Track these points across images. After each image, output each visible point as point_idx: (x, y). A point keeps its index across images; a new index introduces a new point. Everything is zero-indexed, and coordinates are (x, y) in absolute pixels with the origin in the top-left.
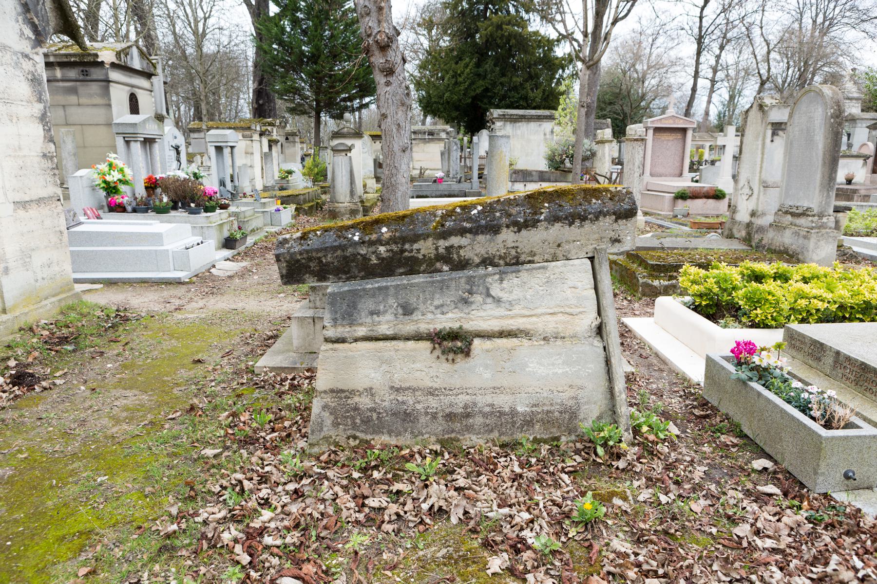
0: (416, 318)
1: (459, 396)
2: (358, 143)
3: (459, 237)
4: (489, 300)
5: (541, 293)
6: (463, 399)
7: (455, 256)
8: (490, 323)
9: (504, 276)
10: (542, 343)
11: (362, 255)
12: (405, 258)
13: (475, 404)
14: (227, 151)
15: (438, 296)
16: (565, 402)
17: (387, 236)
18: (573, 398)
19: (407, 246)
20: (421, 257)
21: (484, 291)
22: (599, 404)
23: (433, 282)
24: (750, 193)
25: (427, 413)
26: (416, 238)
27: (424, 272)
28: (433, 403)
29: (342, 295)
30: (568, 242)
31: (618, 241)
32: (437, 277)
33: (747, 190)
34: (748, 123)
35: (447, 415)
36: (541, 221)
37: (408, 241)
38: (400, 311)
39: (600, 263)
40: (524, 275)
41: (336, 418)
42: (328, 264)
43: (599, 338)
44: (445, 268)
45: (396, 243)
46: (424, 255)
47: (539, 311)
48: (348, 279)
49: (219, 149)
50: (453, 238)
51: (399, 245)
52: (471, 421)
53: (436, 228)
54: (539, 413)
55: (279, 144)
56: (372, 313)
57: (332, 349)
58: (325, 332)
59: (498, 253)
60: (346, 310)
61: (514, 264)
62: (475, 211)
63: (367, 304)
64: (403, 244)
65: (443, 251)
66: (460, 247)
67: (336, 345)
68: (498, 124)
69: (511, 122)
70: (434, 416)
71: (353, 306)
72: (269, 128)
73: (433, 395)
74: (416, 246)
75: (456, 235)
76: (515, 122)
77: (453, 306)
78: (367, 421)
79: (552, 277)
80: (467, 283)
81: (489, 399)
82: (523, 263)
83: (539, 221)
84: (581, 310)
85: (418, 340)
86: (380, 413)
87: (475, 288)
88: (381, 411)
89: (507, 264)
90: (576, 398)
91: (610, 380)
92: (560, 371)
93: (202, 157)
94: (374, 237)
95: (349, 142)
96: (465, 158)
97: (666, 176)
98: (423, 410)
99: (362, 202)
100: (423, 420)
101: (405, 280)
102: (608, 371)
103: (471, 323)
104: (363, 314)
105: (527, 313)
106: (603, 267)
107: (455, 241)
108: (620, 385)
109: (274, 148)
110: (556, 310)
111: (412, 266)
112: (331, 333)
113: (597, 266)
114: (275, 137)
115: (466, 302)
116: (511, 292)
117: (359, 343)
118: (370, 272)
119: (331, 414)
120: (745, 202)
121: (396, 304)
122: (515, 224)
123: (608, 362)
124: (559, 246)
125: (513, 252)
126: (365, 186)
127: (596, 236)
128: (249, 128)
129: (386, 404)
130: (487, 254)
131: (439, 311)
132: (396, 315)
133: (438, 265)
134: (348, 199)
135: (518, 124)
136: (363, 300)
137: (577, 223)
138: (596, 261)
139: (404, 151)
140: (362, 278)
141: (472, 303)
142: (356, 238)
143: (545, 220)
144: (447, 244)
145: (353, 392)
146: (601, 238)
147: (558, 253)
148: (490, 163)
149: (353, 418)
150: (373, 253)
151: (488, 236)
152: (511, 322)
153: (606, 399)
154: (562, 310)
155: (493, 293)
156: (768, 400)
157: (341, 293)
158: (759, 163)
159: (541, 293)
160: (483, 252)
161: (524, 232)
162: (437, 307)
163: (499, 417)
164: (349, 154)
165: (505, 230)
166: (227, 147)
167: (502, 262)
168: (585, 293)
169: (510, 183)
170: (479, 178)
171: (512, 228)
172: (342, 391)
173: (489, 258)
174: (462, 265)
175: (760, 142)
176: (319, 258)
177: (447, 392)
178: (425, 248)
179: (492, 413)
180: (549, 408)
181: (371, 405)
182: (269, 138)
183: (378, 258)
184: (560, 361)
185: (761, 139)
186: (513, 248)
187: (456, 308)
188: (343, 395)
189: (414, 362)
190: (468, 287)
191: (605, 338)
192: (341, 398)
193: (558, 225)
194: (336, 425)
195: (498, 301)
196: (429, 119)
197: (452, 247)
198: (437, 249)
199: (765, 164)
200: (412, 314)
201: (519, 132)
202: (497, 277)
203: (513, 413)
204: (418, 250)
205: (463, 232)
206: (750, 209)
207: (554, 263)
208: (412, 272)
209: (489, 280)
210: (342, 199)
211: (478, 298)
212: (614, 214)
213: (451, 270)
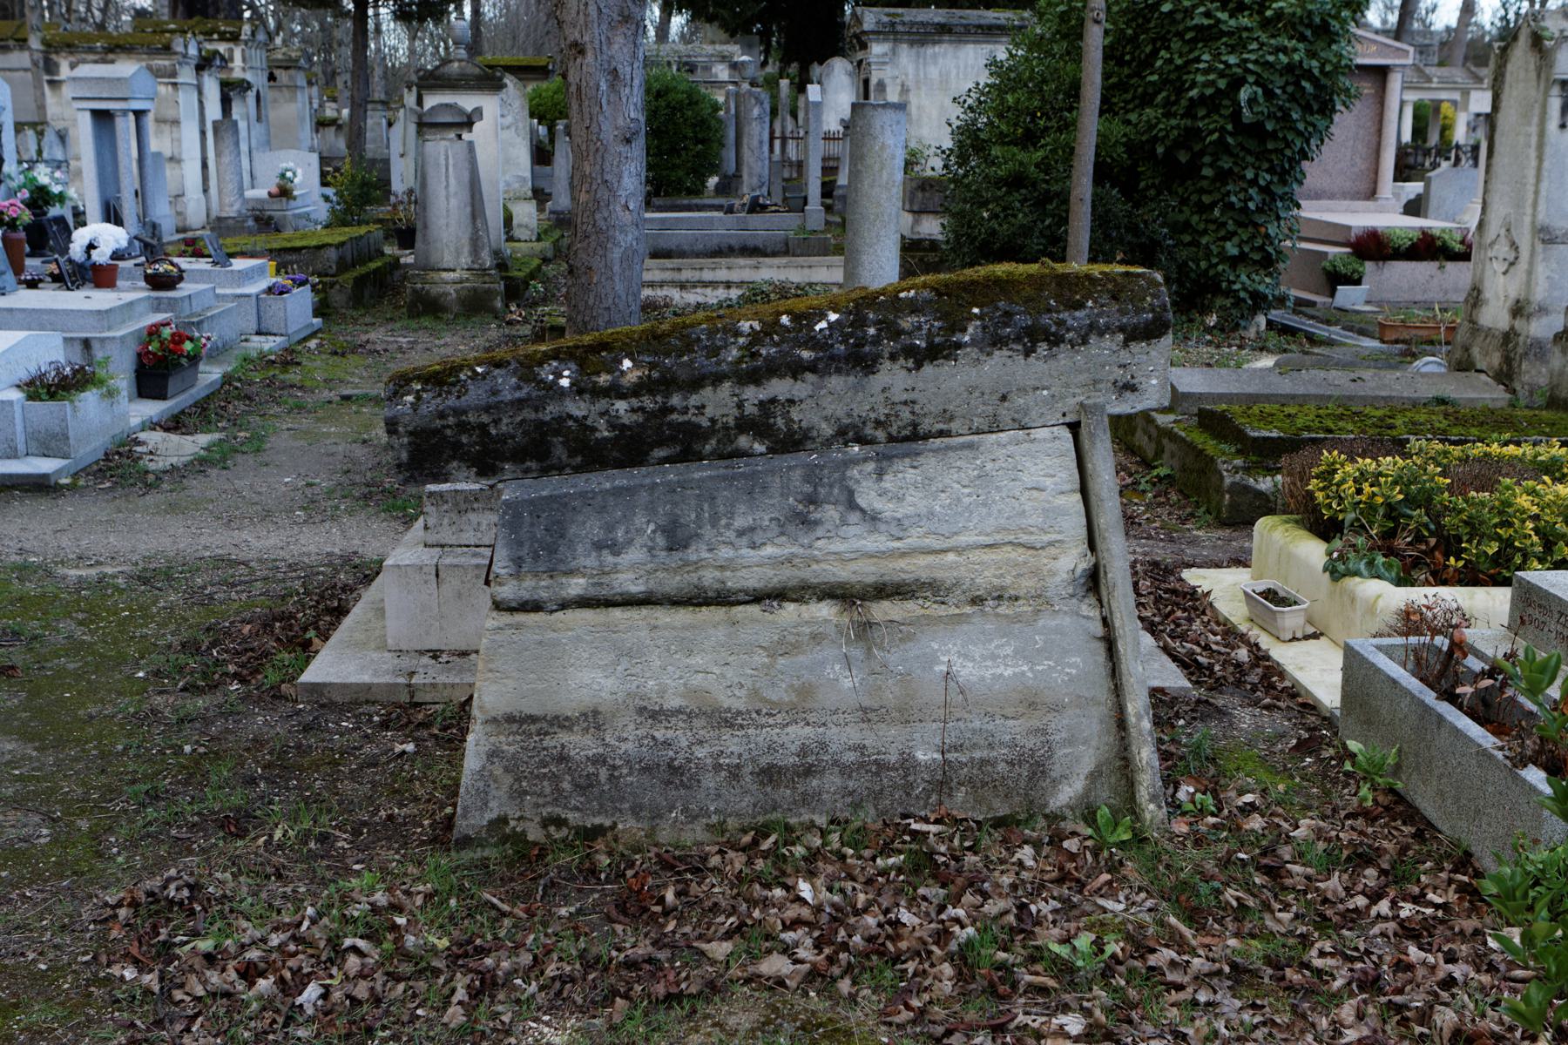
0: (694, 557)
1: (789, 729)
2: (488, 103)
3: (789, 381)
4: (854, 517)
5: (966, 500)
6: (798, 733)
7: (780, 422)
8: (854, 566)
9: (885, 464)
10: (968, 609)
11: (576, 420)
12: (671, 425)
13: (823, 746)
14: (125, 127)
15: (742, 508)
16: (1020, 740)
17: (633, 377)
18: (1037, 730)
19: (676, 400)
20: (705, 423)
21: (843, 498)
22: (1094, 743)
23: (733, 478)
24: (1511, 258)
25: (718, 767)
26: (696, 384)
27: (709, 457)
28: (733, 744)
29: (537, 507)
30: (1022, 390)
31: (1130, 387)
32: (742, 466)
33: (1503, 249)
34: (1508, 77)
35: (763, 771)
36: (966, 345)
37: (680, 388)
38: (661, 541)
39: (1092, 435)
40: (930, 463)
41: (518, 780)
42: (502, 439)
43: (1092, 600)
44: (759, 447)
45: (652, 392)
46: (713, 421)
47: (964, 539)
48: (545, 472)
49: (103, 118)
50: (775, 381)
51: (659, 399)
52: (815, 783)
53: (740, 360)
54: (962, 765)
55: (251, 95)
56: (599, 546)
57: (510, 626)
58: (495, 588)
59: (873, 415)
60: (539, 539)
61: (906, 439)
62: (823, 325)
63: (589, 527)
64: (667, 396)
65: (755, 410)
66: (791, 402)
67: (520, 617)
68: (877, 49)
69: (912, 43)
70: (734, 773)
71: (558, 531)
72: (222, 48)
73: (732, 726)
74: (694, 400)
75: (781, 377)
76: (923, 43)
77: (777, 530)
78: (586, 786)
79: (989, 466)
80: (807, 479)
81: (853, 734)
82: (926, 437)
83: (959, 345)
84: (1054, 537)
85: (700, 605)
86: (614, 767)
87: (822, 491)
88: (618, 762)
89: (891, 439)
90: (1044, 732)
91: (1118, 690)
92: (1008, 672)
93: (40, 134)
94: (604, 379)
95: (467, 101)
96: (784, 140)
97: (1332, 197)
98: (709, 761)
99: (502, 266)
100: (710, 781)
101: (672, 473)
102: (1114, 670)
103: (815, 567)
104: (580, 548)
105: (936, 543)
106: (1099, 445)
107: (779, 388)
108: (1137, 707)
109: (237, 111)
110: (998, 538)
111: (688, 444)
112: (507, 591)
113: (1086, 444)
114: (237, 74)
115: (806, 522)
116: (900, 499)
117: (569, 612)
118: (592, 454)
119: (506, 770)
120: (1502, 279)
121: (652, 527)
122: (909, 351)
123: (1110, 643)
124: (1004, 398)
125: (906, 414)
126: (508, 221)
127: (1083, 378)
128: (167, 49)
129: (629, 746)
130: (849, 415)
131: (744, 540)
132: (651, 549)
133: (743, 441)
134: (465, 260)
135: (930, 50)
136: (580, 518)
137: (1042, 348)
138: (1083, 431)
139: (628, 141)
140: (578, 470)
141: (817, 523)
142: (565, 382)
143: (974, 342)
144: (763, 394)
145: (561, 722)
146: (1095, 382)
147: (1001, 416)
148: (857, 158)
149: (555, 778)
150: (602, 414)
151: (852, 378)
152: (902, 564)
153: (1108, 732)
154: (1011, 538)
155: (861, 501)
156: (1457, 733)
157: (531, 502)
158: (1531, 180)
159: (966, 500)
160: (840, 413)
161: (928, 369)
162: (741, 533)
163: (877, 774)
164: (466, 136)
165: (887, 364)
166: (125, 112)
167: (880, 435)
168: (1061, 501)
169: (909, 218)
170: (824, 195)
171: (902, 361)
172: (533, 719)
173: (854, 426)
174: (791, 442)
175: (1534, 129)
176: (483, 427)
177: (764, 720)
178: (717, 403)
179: (862, 765)
180: (985, 754)
181: (595, 750)
182: (224, 76)
183: (612, 426)
184: (1009, 650)
185: (1535, 120)
186: (905, 403)
187: (782, 534)
188: (533, 728)
189: (690, 653)
190: (808, 488)
191: (1105, 600)
192: (530, 735)
193: (999, 355)
194: (518, 794)
195: (872, 519)
196: (678, 21)
197: (773, 401)
198: (740, 406)
199: (1544, 185)
200: (686, 547)
201: (933, 72)
202: (870, 466)
203: (907, 764)
204: (701, 408)
205: (797, 370)
206: (1513, 295)
207: (994, 436)
208: (688, 455)
209: (854, 472)
210: (448, 259)
211: (830, 513)
212: (1122, 329)
213: (771, 450)
